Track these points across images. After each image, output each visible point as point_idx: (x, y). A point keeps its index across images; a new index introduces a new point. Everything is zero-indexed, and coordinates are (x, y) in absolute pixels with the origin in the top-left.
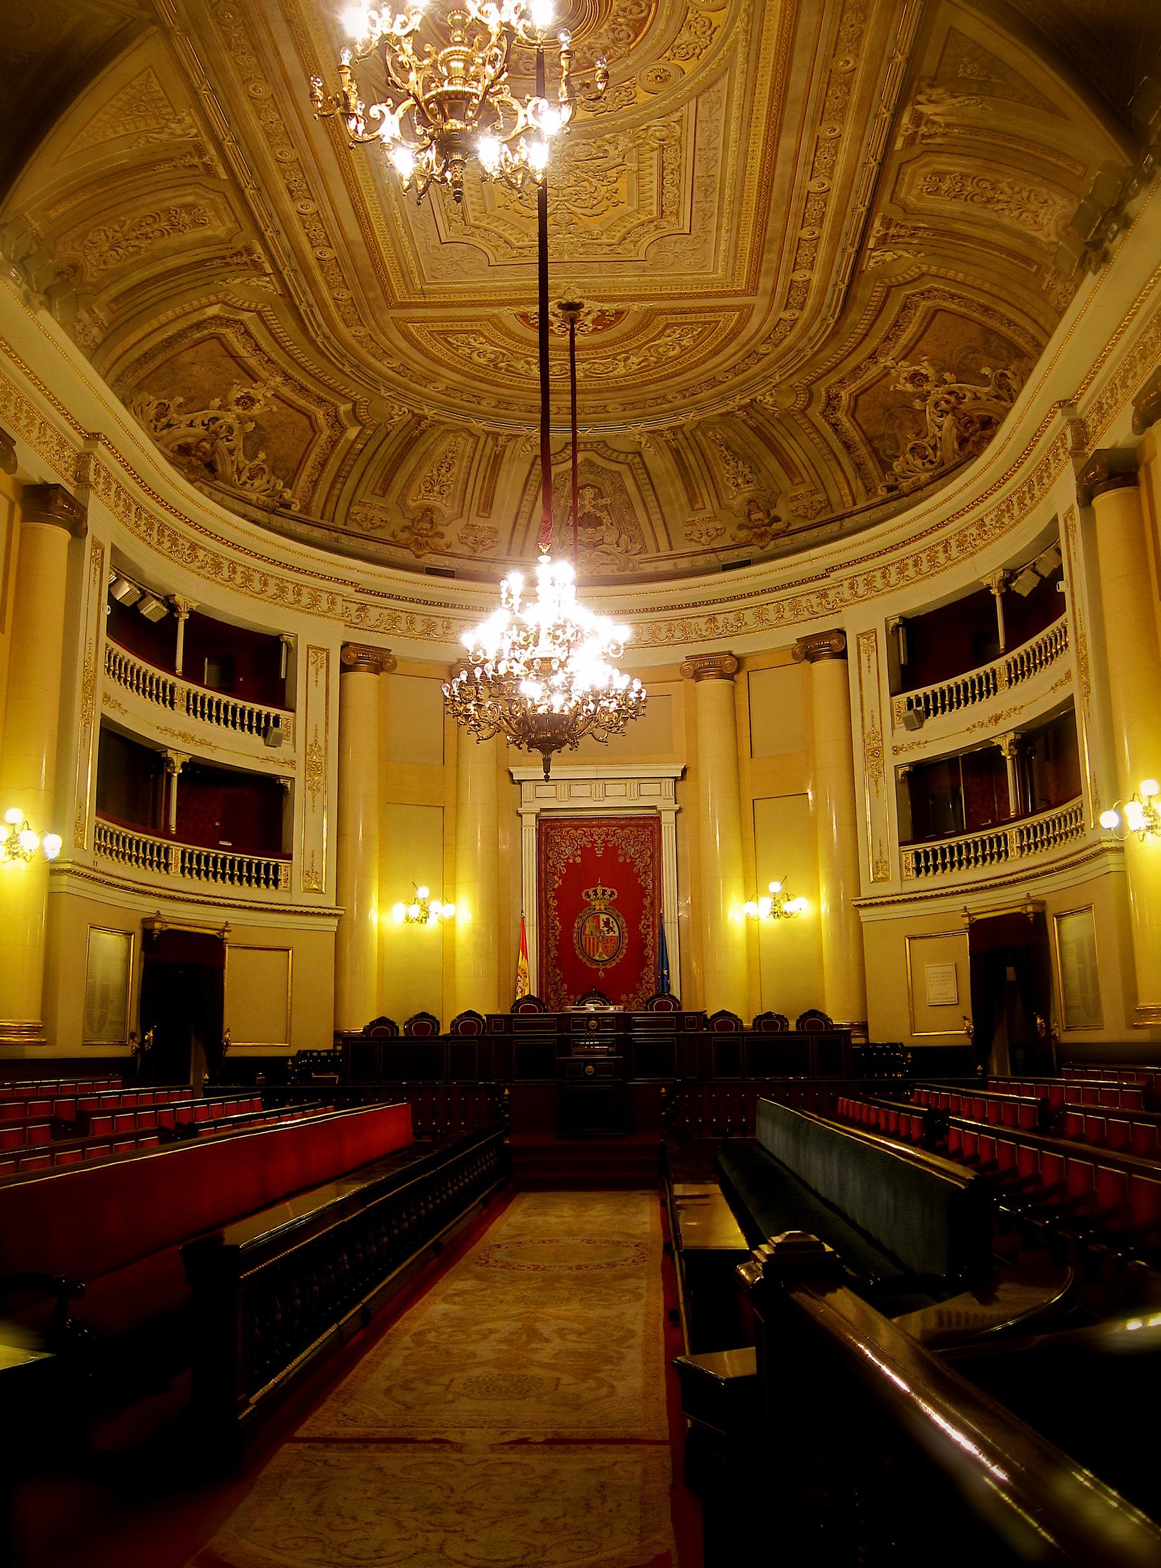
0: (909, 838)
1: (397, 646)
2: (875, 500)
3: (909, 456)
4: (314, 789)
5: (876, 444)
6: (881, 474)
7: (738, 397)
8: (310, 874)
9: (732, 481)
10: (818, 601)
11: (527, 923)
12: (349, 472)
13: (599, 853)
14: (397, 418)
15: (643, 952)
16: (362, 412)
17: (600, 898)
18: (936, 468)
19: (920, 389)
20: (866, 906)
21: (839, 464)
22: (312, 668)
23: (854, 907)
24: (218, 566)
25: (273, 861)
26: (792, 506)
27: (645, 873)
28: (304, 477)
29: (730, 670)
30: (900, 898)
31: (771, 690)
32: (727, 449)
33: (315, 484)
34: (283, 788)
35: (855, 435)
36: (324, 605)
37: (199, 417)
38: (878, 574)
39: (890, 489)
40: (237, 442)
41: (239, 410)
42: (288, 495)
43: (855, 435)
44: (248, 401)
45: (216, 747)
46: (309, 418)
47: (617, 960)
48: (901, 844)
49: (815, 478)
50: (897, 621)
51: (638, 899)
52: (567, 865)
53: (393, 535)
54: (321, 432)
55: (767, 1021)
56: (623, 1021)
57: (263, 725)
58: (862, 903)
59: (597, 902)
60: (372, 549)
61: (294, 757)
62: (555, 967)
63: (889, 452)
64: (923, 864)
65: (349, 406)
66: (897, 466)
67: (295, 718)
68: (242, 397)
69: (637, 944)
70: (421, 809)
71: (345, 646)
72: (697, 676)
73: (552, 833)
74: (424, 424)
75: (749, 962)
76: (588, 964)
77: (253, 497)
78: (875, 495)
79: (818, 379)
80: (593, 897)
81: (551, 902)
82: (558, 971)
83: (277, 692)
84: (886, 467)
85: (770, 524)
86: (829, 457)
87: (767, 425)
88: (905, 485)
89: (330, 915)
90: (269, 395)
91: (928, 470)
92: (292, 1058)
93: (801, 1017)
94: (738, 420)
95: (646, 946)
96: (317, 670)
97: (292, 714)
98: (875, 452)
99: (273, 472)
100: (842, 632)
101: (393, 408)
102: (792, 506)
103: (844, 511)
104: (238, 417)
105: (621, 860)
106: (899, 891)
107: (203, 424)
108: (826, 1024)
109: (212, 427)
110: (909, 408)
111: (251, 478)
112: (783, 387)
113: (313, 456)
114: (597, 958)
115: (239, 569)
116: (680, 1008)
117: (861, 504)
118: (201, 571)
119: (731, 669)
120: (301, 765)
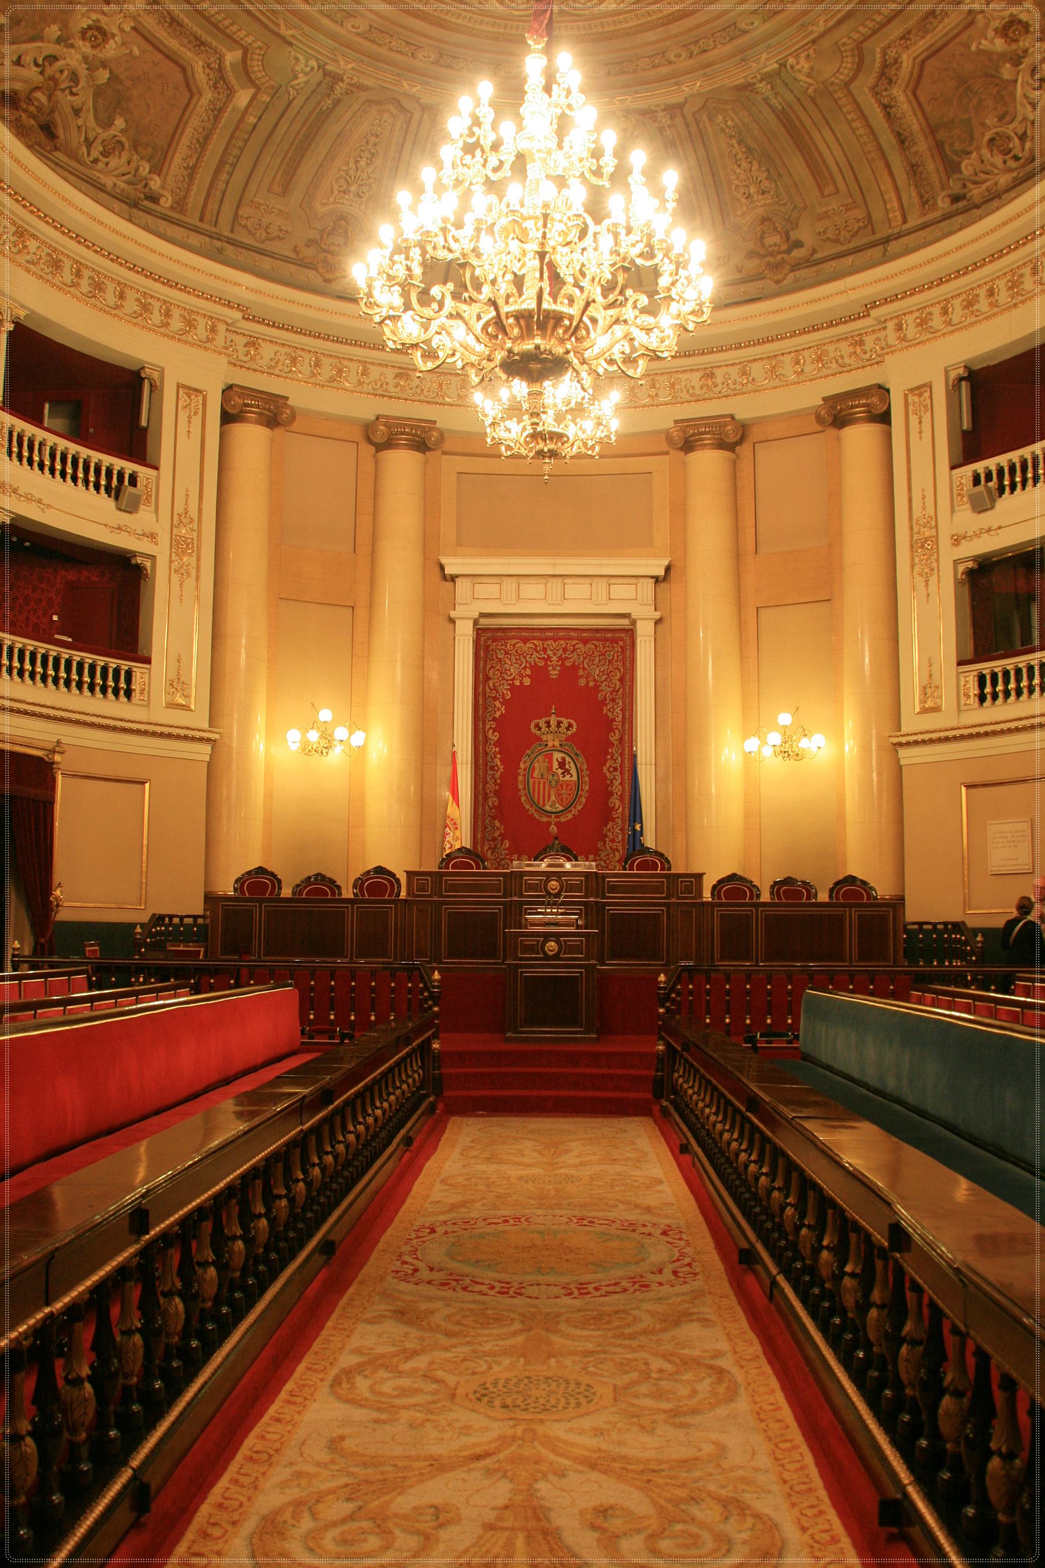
0: (969, 654)
1: (300, 395)
2: (931, 216)
3: (985, 152)
4: (183, 573)
5: (941, 135)
6: (944, 179)
7: (764, 56)
8: (178, 683)
9: (742, 191)
10: (851, 349)
11: (459, 761)
12: (238, 157)
13: (554, 674)
14: (302, 78)
15: (608, 804)
16: (255, 66)
17: (554, 732)
18: (1023, 166)
19: (1014, 46)
20: (908, 744)
21: (888, 165)
22: (183, 415)
23: (893, 746)
24: (56, 265)
25: (125, 665)
26: (819, 227)
27: (613, 700)
28: (177, 160)
29: (732, 439)
30: (957, 733)
31: (776, 465)
32: (740, 143)
33: (192, 171)
34: (139, 569)
35: (913, 123)
36: (201, 332)
37: (31, 50)
38: (936, 310)
39: (955, 199)
40: (84, 97)
41: (86, 48)
42: (156, 183)
43: (913, 123)
44: (97, 34)
45: (49, 506)
46: (183, 69)
47: (574, 812)
48: (960, 663)
49: (854, 186)
50: (961, 371)
51: (602, 733)
52: (513, 688)
53: (295, 250)
54: (201, 94)
55: (789, 888)
56: (593, 882)
57: (115, 482)
58: (903, 740)
59: (550, 737)
60: (268, 267)
61: (157, 530)
62: (493, 818)
63: (958, 146)
64: (988, 689)
65: (238, 54)
66: (967, 168)
67: (158, 478)
68: (90, 28)
69: (600, 792)
70: (323, 594)
71: (228, 389)
72: (688, 446)
73: (493, 646)
74: (340, 88)
75: (747, 815)
76: (536, 816)
77: (109, 181)
78: (934, 207)
79: (875, 32)
80: (544, 729)
81: (490, 734)
82: (497, 824)
83: (134, 442)
84: (952, 167)
85: (788, 252)
86: (874, 155)
87: (797, 108)
88: (976, 193)
89: (201, 740)
90: (127, 28)
91: (1011, 170)
92: (142, 926)
93: (837, 883)
94: (759, 97)
95: (612, 794)
96: (190, 417)
97: (154, 472)
98: (939, 146)
99: (135, 147)
100: (883, 390)
101: (297, 59)
102: (819, 227)
103: (890, 231)
104: (85, 58)
105: (582, 682)
106: (955, 724)
107: (37, 65)
108: (869, 895)
109: (49, 71)
110: (991, 76)
111: (105, 154)
112: (826, 43)
113: (189, 131)
114: (548, 808)
115: (86, 273)
116: (669, 869)
117: (913, 222)
118: (32, 267)
119: (732, 438)
120: (164, 539)
